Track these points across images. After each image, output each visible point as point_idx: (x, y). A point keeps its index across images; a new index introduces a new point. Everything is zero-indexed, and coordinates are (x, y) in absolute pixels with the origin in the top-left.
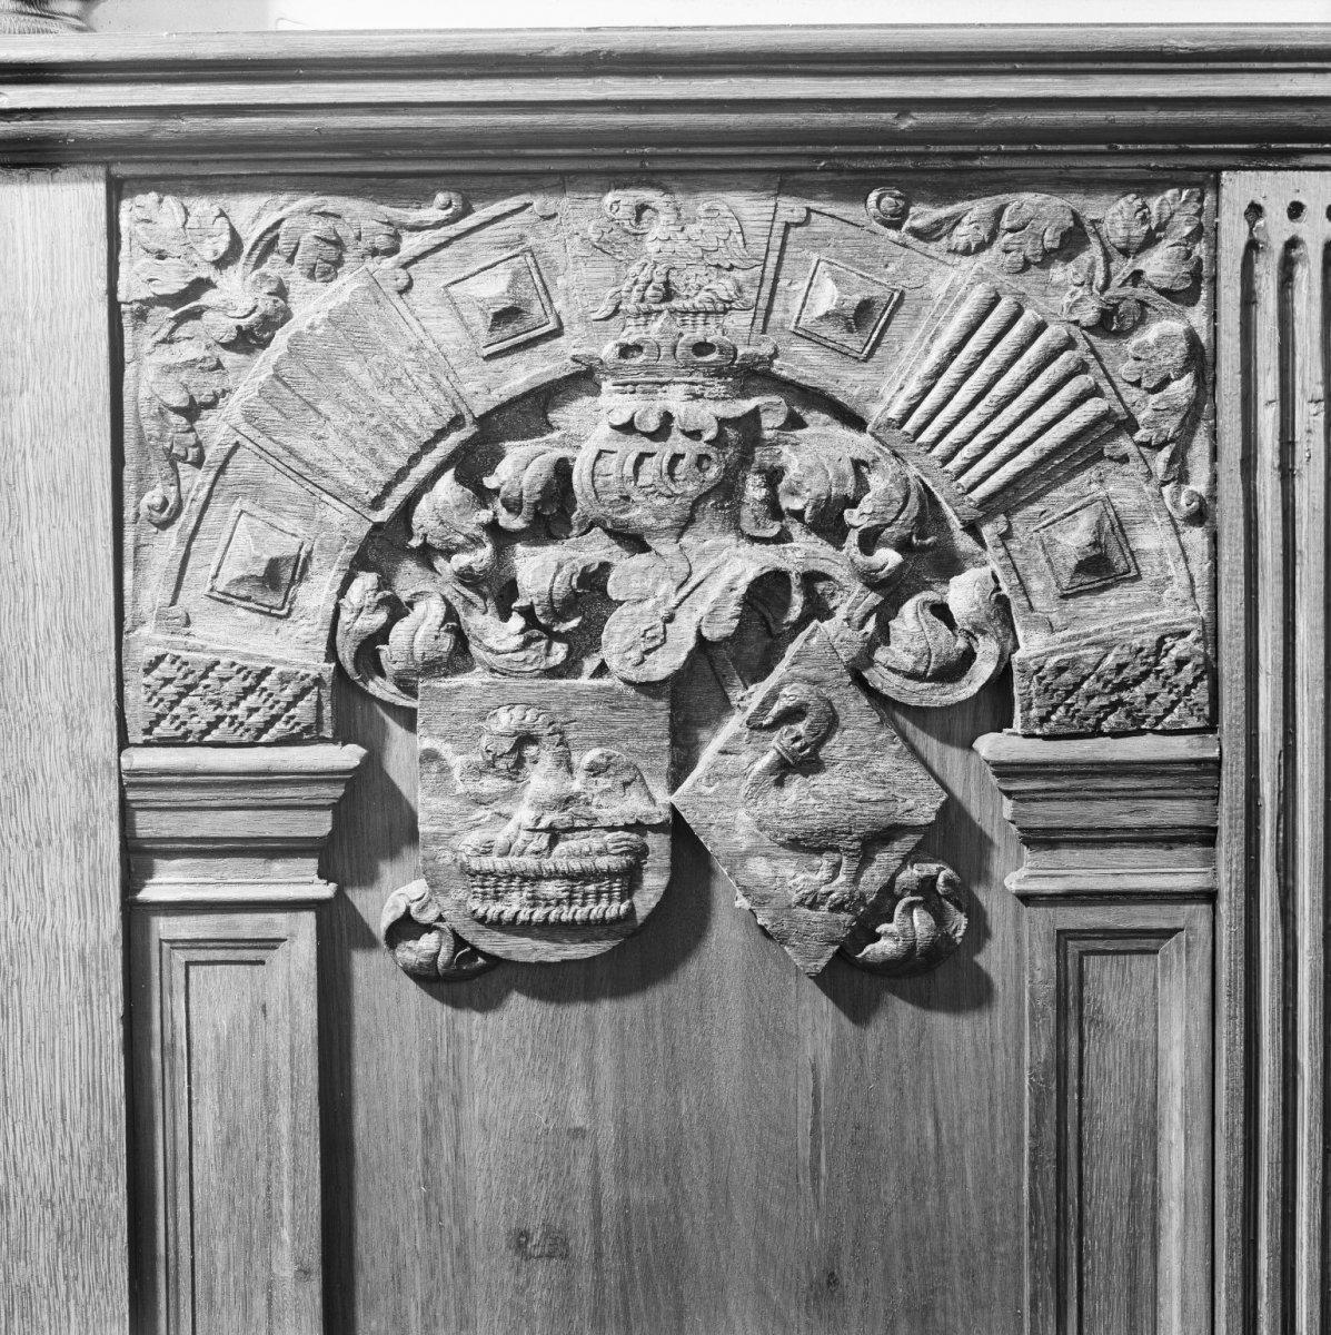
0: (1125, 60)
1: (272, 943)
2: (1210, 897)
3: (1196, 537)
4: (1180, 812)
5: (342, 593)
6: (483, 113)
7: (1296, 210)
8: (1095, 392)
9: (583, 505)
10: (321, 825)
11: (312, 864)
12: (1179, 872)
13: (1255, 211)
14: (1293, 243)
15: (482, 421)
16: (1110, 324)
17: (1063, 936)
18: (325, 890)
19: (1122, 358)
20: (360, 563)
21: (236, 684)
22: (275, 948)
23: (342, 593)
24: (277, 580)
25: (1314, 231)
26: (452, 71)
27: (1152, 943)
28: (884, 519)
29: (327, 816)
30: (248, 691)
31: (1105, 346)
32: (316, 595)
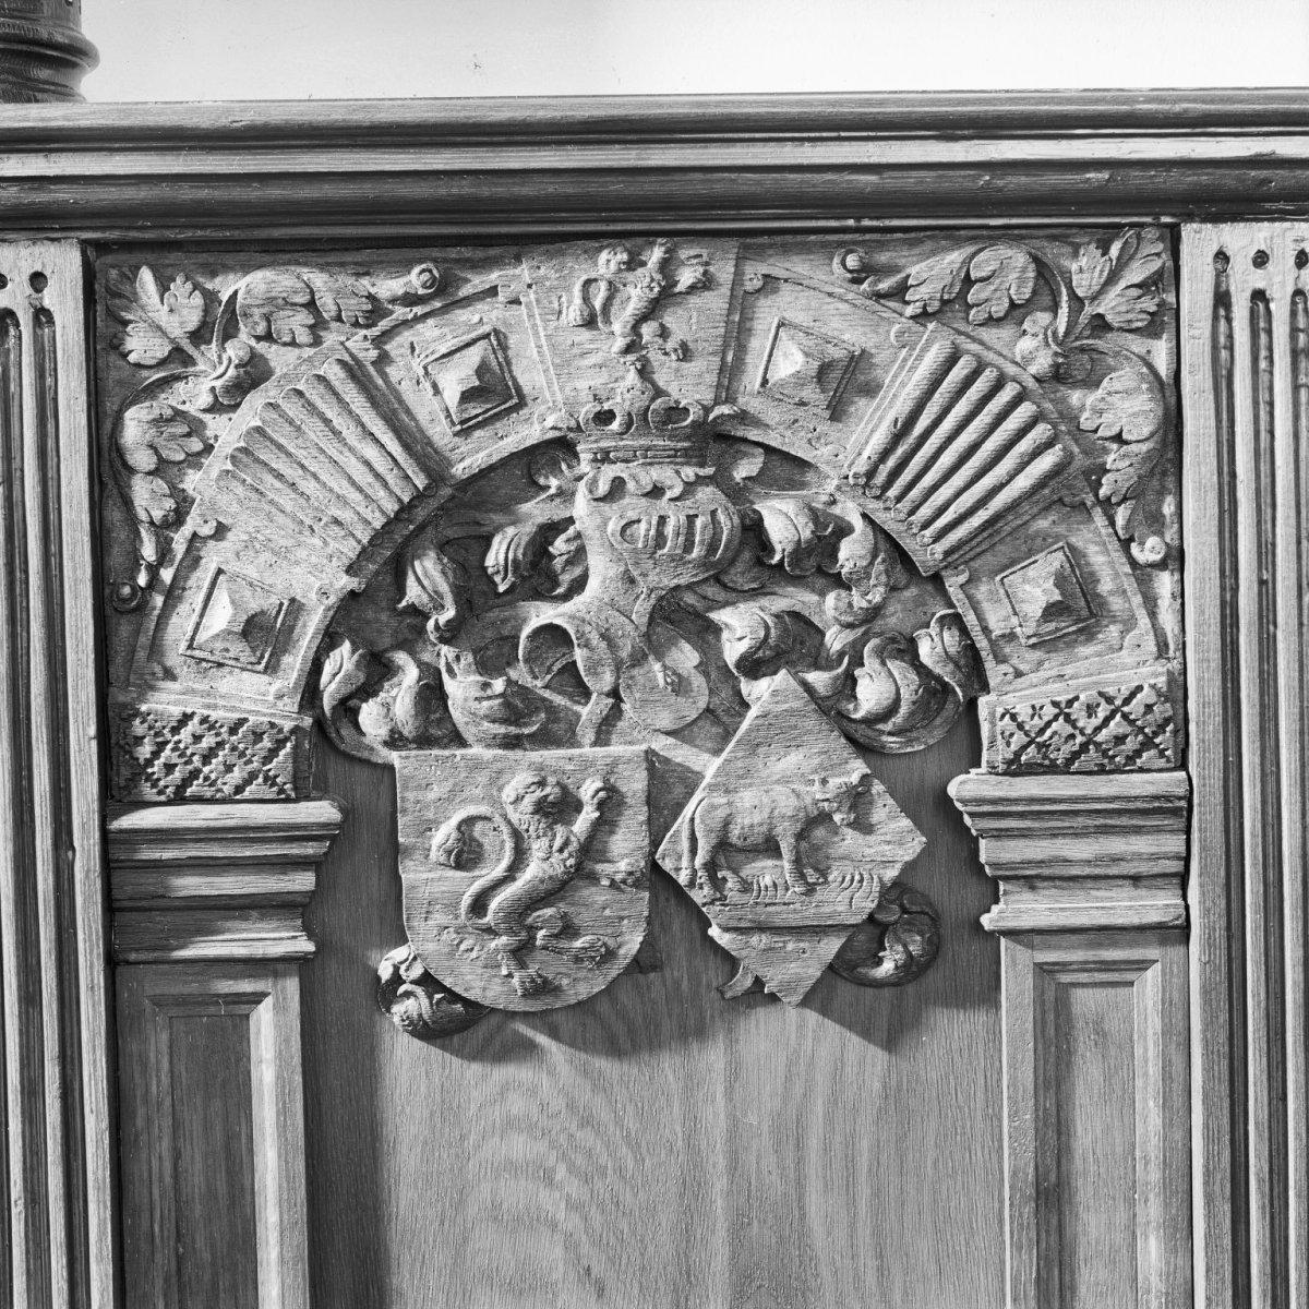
7: (38, 280)
24: (263, 634)
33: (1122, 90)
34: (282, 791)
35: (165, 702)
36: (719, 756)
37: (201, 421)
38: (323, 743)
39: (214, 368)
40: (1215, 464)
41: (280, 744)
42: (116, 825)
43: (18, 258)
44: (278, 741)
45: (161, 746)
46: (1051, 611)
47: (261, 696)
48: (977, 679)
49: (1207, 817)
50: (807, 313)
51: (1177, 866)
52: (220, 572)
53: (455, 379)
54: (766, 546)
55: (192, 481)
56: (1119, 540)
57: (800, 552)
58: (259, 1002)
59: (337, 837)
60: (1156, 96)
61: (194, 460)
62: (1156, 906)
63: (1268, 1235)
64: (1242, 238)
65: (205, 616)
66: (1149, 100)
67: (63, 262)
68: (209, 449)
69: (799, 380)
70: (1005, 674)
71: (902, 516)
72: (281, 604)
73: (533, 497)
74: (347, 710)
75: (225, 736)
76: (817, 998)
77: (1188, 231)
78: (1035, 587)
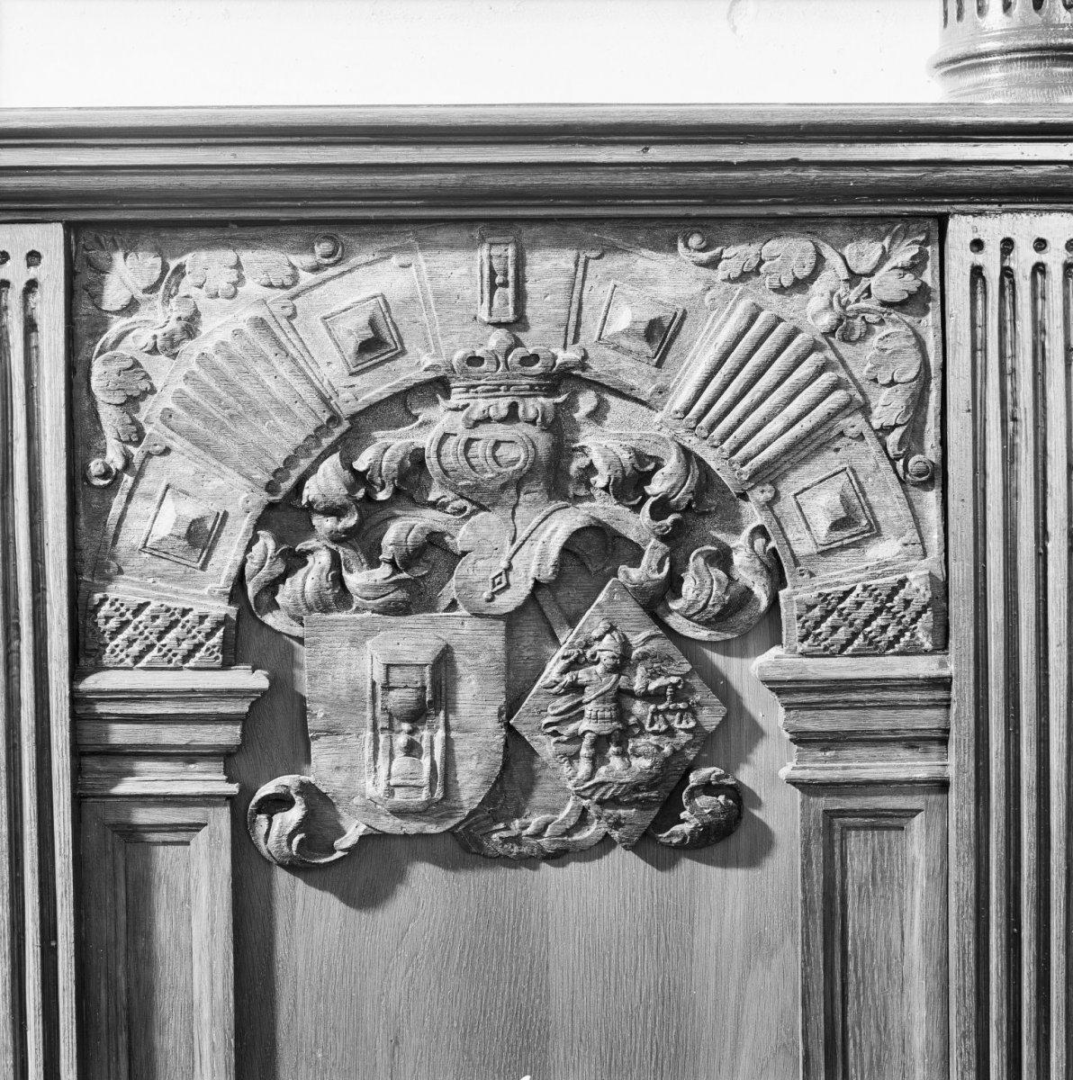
0: (184, 137)
1: (197, 827)
2: (942, 786)
3: (930, 500)
4: (928, 719)
5: (248, 549)
6: (394, 174)
7: (33, 257)
8: (835, 386)
9: (727, 477)
10: (228, 735)
11: (220, 766)
12: (918, 766)
13: (1008, 245)
14: (31, 286)
15: (353, 417)
16: (843, 330)
17: (829, 815)
18: (233, 789)
19: (861, 358)
20: (261, 523)
21: (869, 606)
22: (198, 831)
23: (248, 549)
24: (200, 538)
25: (1055, 259)
26: (534, 139)
27: (183, 836)
28: (148, 496)
29: (238, 729)
30: (878, 611)
31: (845, 350)
32: (227, 556)
35: (123, 591)
37: (657, 520)
38: (241, 635)
40: (972, 532)
42: (83, 686)
43: (16, 238)
44: (827, 611)
45: (125, 624)
46: (836, 526)
49: (963, 693)
50: (641, 283)
52: (168, 487)
56: (889, 458)
59: (259, 700)
62: (918, 766)
63: (1004, 996)
64: (994, 227)
65: (149, 519)
66: (1001, 904)
67: (50, 238)
69: (627, 333)
71: (726, 454)
72: (218, 514)
73: (408, 424)
75: (129, 615)
76: (634, 848)
77: (953, 224)
78: (822, 506)
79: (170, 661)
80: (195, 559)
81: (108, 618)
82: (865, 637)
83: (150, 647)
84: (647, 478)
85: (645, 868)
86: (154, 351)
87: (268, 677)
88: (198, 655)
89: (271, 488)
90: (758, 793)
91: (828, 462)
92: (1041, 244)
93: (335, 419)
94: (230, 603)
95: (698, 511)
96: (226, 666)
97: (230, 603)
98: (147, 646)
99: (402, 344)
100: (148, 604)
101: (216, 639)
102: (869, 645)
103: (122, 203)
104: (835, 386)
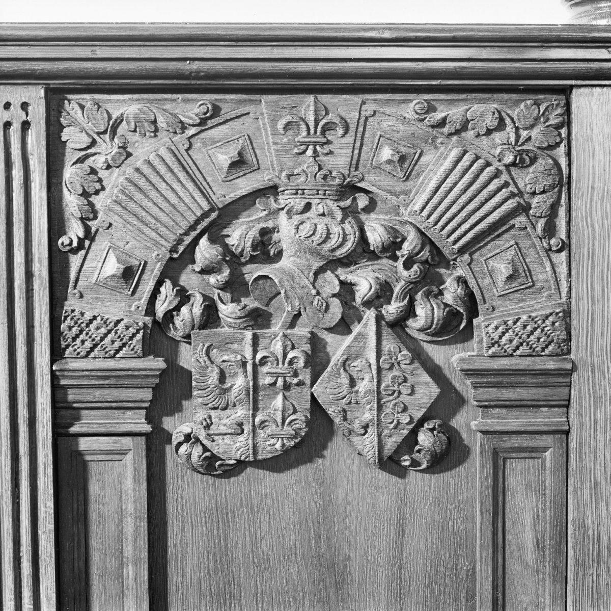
8: (513, 195)
33: (314, 24)
34: (136, 353)
36: (505, 125)
38: (157, 335)
39: (106, 150)
41: (138, 331)
43: (17, 94)
46: (510, 278)
47: (125, 311)
48: (473, 312)
51: (569, 384)
53: (224, 158)
54: (368, 244)
55: (96, 200)
57: (384, 249)
58: (126, 454)
60: (542, 28)
61: (97, 193)
67: (36, 95)
68: (103, 189)
70: (488, 309)
74: (169, 316)
79: (78, 354)
80: (525, 279)
81: (70, 328)
82: (528, 344)
83: (124, 345)
84: (399, 246)
85: (202, 480)
86: (109, 167)
87: (164, 361)
88: (96, 350)
89: (173, 250)
90: (458, 430)
91: (507, 241)
92: (24, 106)
93: (212, 210)
94: (370, 309)
95: (432, 264)
96: (145, 355)
97: (370, 309)
98: (94, 345)
99: (258, 164)
100: (122, 320)
101: (139, 336)
102: (501, 349)
103: (70, 72)
104: (513, 195)
